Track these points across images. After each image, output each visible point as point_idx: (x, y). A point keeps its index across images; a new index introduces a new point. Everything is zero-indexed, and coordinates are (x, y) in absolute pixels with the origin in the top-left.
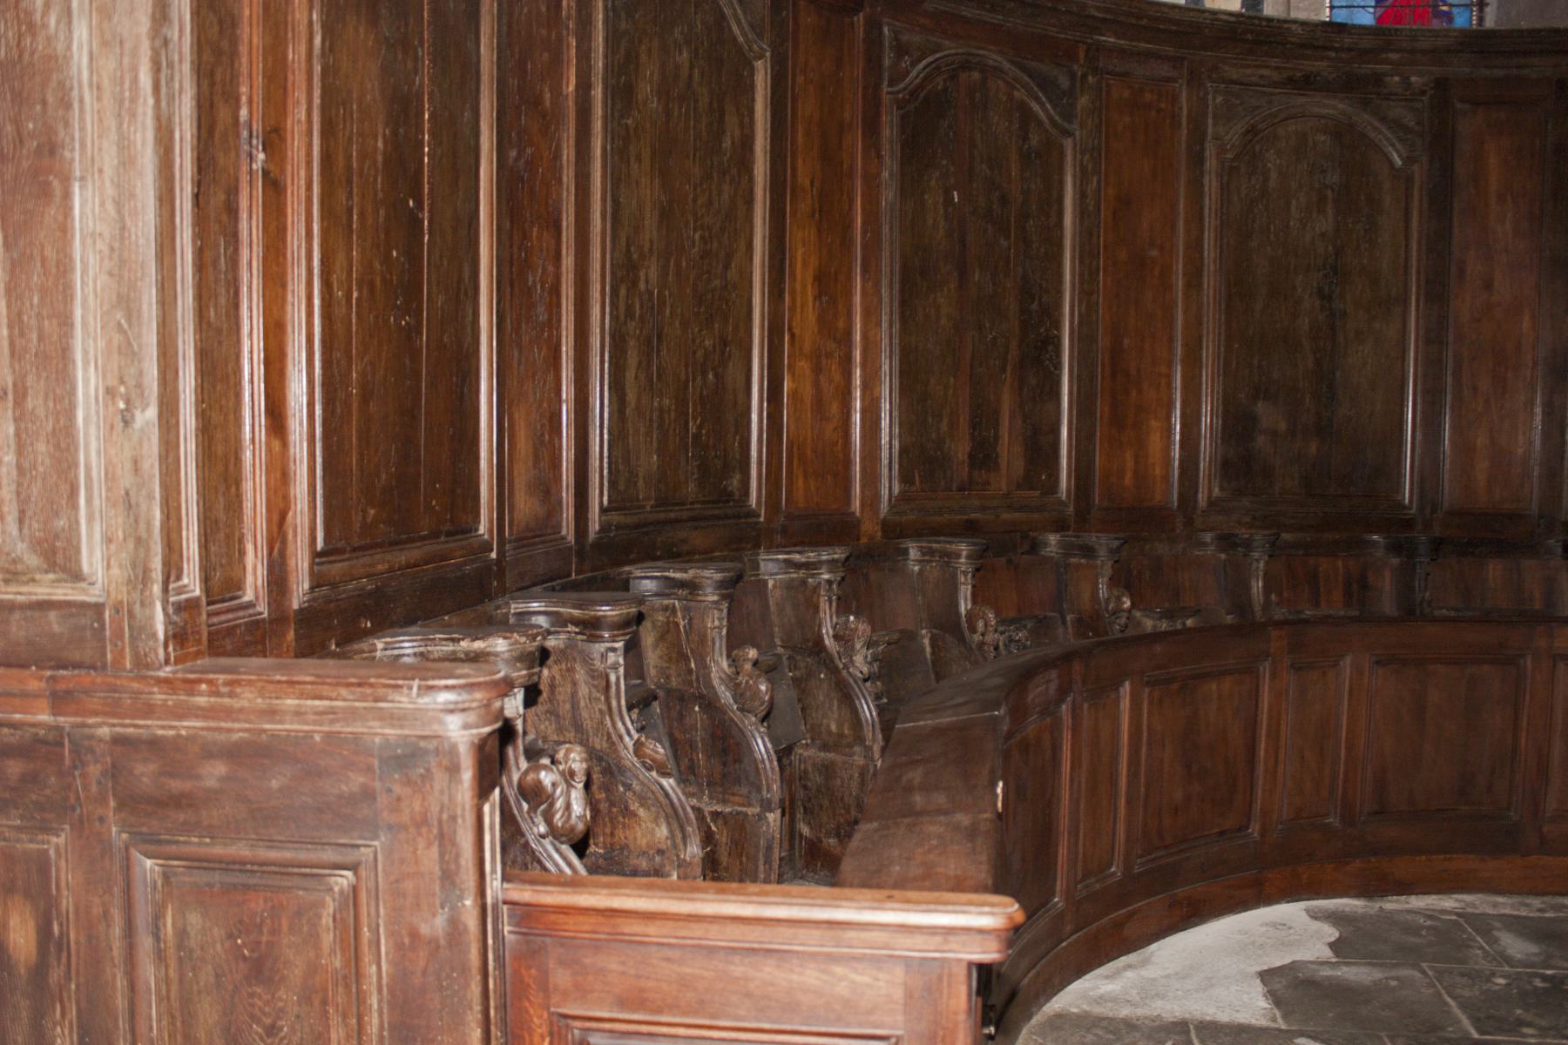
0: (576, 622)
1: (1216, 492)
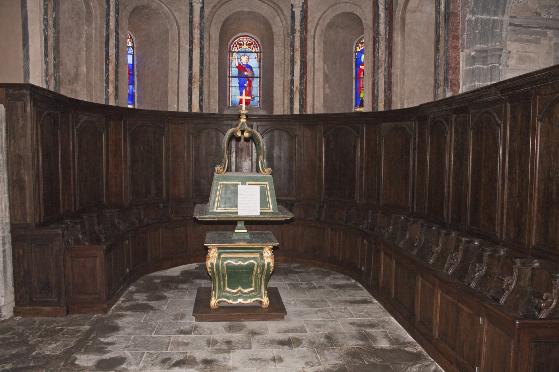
0: (74, 222)
1: (194, 195)
